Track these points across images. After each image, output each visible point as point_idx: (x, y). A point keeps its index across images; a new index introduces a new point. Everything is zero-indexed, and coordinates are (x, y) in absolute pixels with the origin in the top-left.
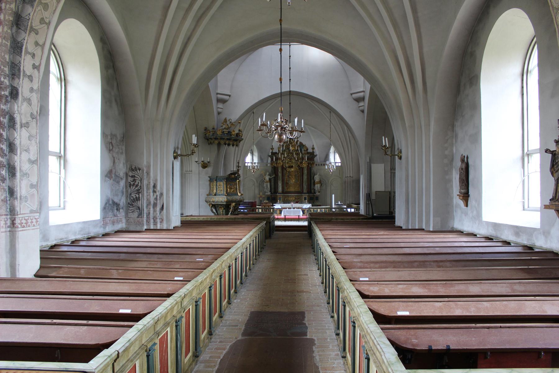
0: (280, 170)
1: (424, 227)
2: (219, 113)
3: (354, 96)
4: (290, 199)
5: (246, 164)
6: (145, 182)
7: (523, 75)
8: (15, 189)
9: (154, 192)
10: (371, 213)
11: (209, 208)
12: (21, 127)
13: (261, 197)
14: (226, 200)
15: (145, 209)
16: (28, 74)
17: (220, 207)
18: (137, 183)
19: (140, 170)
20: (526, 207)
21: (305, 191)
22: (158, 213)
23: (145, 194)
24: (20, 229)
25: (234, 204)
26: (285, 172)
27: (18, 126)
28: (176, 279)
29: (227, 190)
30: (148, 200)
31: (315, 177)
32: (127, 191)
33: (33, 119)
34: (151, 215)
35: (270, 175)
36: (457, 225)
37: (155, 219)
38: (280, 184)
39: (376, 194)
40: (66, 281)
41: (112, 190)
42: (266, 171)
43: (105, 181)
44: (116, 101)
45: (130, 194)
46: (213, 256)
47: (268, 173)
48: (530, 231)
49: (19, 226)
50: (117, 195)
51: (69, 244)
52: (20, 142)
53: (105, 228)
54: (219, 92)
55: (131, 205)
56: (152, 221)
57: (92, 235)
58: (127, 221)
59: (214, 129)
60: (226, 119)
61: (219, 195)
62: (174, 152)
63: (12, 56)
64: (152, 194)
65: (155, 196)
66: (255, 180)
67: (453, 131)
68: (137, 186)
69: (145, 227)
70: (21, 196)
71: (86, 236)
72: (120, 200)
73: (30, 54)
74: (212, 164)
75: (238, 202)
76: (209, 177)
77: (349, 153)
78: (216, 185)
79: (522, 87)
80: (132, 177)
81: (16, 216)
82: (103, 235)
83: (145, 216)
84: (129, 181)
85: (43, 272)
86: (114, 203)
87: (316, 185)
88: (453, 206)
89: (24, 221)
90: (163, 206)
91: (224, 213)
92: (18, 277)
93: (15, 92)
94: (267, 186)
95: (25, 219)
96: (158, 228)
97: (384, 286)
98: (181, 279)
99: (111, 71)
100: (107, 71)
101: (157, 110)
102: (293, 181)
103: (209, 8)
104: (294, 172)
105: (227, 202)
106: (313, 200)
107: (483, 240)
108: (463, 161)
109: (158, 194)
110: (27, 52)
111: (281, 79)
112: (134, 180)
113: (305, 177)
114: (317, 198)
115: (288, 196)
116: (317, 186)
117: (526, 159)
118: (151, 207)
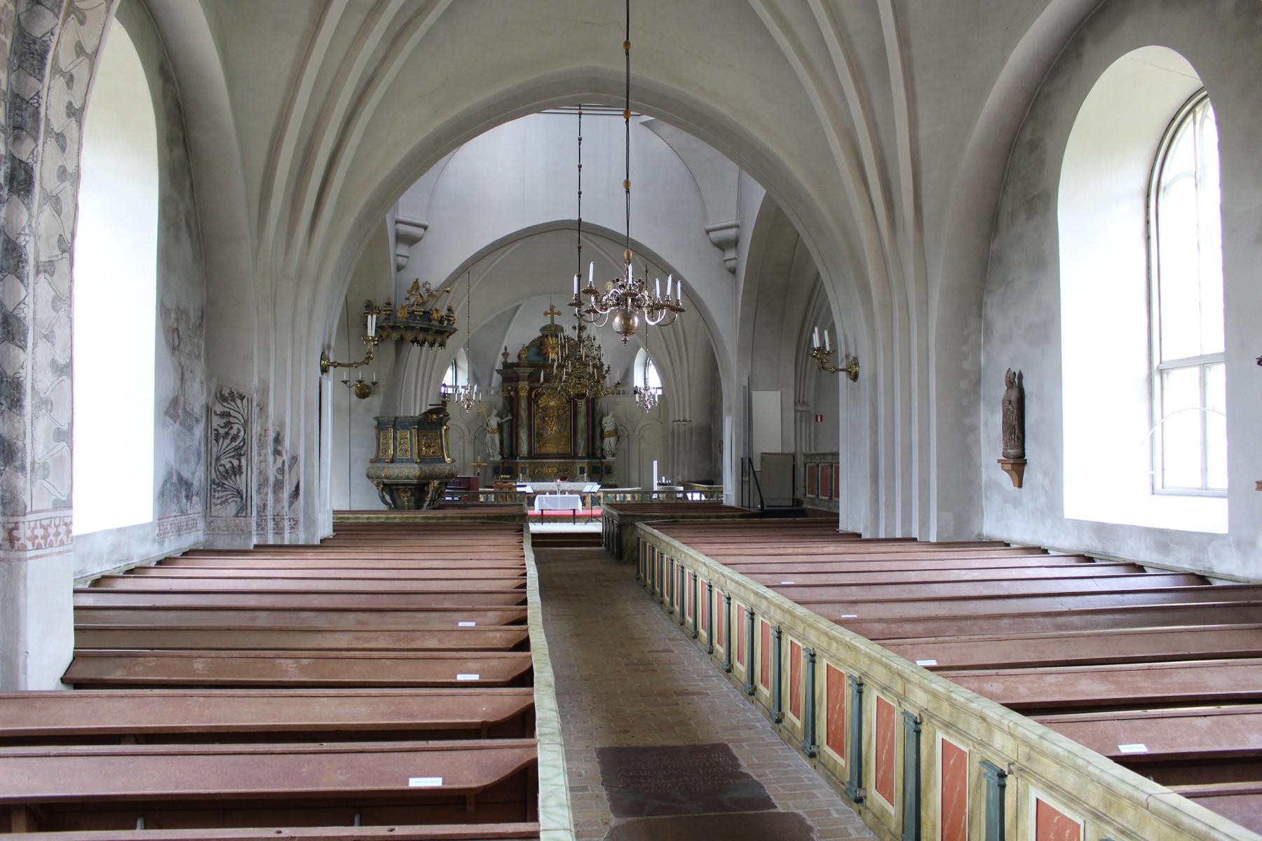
0: (523, 404)
1: (915, 534)
2: (399, 268)
3: (712, 235)
4: (545, 470)
5: (443, 389)
6: (256, 429)
7: (1148, 196)
8: (20, 443)
9: (277, 452)
10: (746, 503)
11: (375, 492)
12: (38, 273)
13: (479, 466)
14: (417, 473)
15: (254, 496)
16: (57, 130)
17: (404, 491)
18: (234, 432)
19: (242, 398)
20: (1158, 486)
21: (581, 452)
22: (286, 505)
23: (255, 458)
24: (29, 554)
25: (436, 483)
26: (534, 407)
27: (30, 268)
28: (461, 678)
29: (420, 450)
30: (260, 473)
31: (605, 420)
32: (209, 451)
33: (64, 252)
34: (270, 511)
35: (499, 415)
36: (990, 528)
37: (278, 519)
38: (523, 436)
39: (762, 459)
40: (185, 696)
41: (178, 448)
42: (491, 406)
43: (164, 425)
44: (188, 226)
45: (218, 459)
46: (499, 613)
47: (495, 412)
48: (1202, 541)
49: (30, 546)
50: (187, 461)
51: (86, 587)
52: (35, 314)
53: (161, 543)
54: (401, 218)
55: (218, 485)
56: (271, 524)
57: (135, 562)
58: (209, 525)
59: (389, 304)
60: (416, 282)
61: (402, 461)
62: (323, 357)
63: (13, 76)
64: (271, 458)
65: (279, 464)
66: (463, 427)
67: (980, 316)
68: (234, 438)
69: (255, 541)
70: (33, 463)
71: (123, 566)
72: (193, 474)
73: (63, 74)
74: (382, 389)
75: (447, 477)
76: (376, 418)
77: (681, 363)
78: (395, 438)
79: (1148, 222)
80: (222, 415)
81: (21, 519)
82: (159, 563)
83: (255, 513)
84: (215, 426)
85: (88, 671)
86: (180, 479)
87: (607, 440)
88: (980, 487)
89: (40, 532)
90: (297, 487)
91: (412, 504)
92: (23, 689)
93: (22, 176)
94: (493, 439)
95: (42, 526)
96: (286, 543)
97: (1013, 679)
98: (475, 677)
99: (179, 151)
100: (171, 151)
101: (287, 252)
102: (552, 430)
103: (421, 12)
104: (555, 409)
105: (419, 478)
106: (596, 474)
107: (1072, 561)
108: (1010, 384)
109: (286, 457)
110: (57, 70)
111: (627, 184)
112: (228, 425)
113: (582, 421)
114: (609, 470)
115: (542, 465)
116: (609, 443)
117: (1157, 379)
118: (270, 491)
